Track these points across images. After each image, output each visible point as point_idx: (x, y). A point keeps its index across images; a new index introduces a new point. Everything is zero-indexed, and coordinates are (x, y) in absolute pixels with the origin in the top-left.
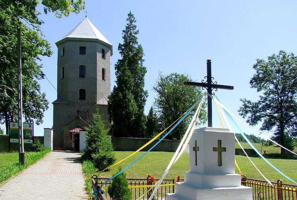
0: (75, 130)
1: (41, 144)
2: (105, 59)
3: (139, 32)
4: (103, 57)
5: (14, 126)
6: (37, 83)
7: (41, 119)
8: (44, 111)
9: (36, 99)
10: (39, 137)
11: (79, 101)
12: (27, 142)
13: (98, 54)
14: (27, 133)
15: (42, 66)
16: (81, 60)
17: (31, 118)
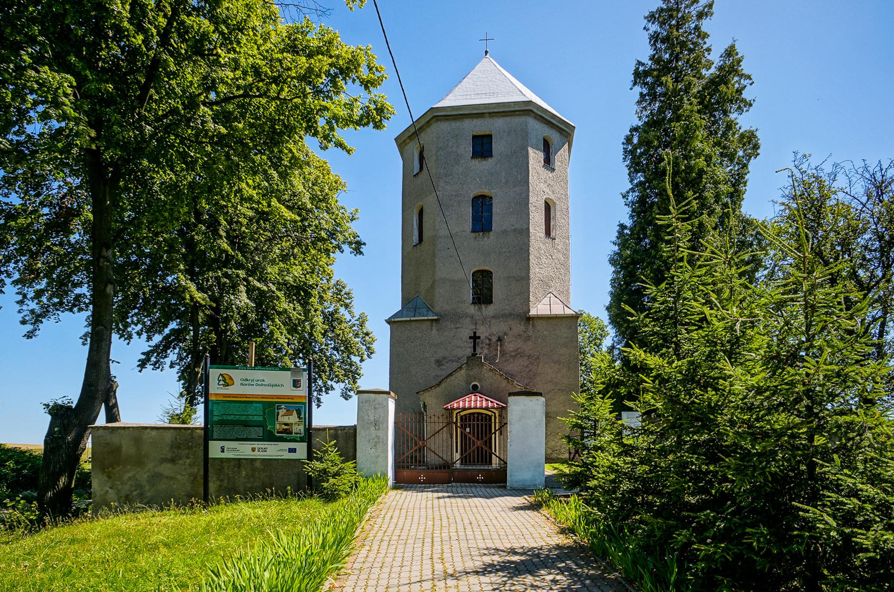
0: (464, 401)
1: (343, 462)
2: (553, 170)
3: (714, 9)
4: (548, 162)
5: (228, 385)
6: (344, 288)
7: (355, 382)
8: (362, 360)
9: (340, 329)
10: (336, 429)
11: (472, 310)
12: (280, 453)
13: (531, 151)
14: (282, 412)
15: (356, 216)
16: (478, 176)
17: (329, 383)
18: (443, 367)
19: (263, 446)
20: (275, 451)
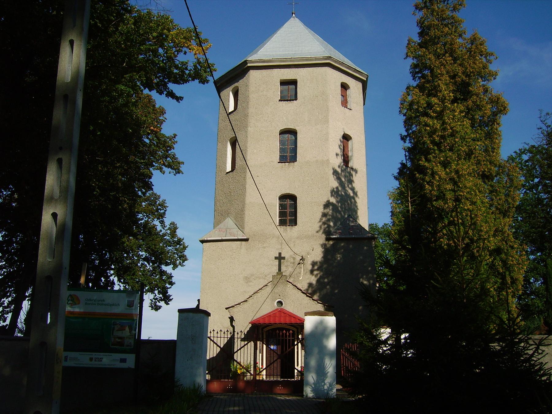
18: (251, 284)
19: (100, 357)
20: (108, 360)
